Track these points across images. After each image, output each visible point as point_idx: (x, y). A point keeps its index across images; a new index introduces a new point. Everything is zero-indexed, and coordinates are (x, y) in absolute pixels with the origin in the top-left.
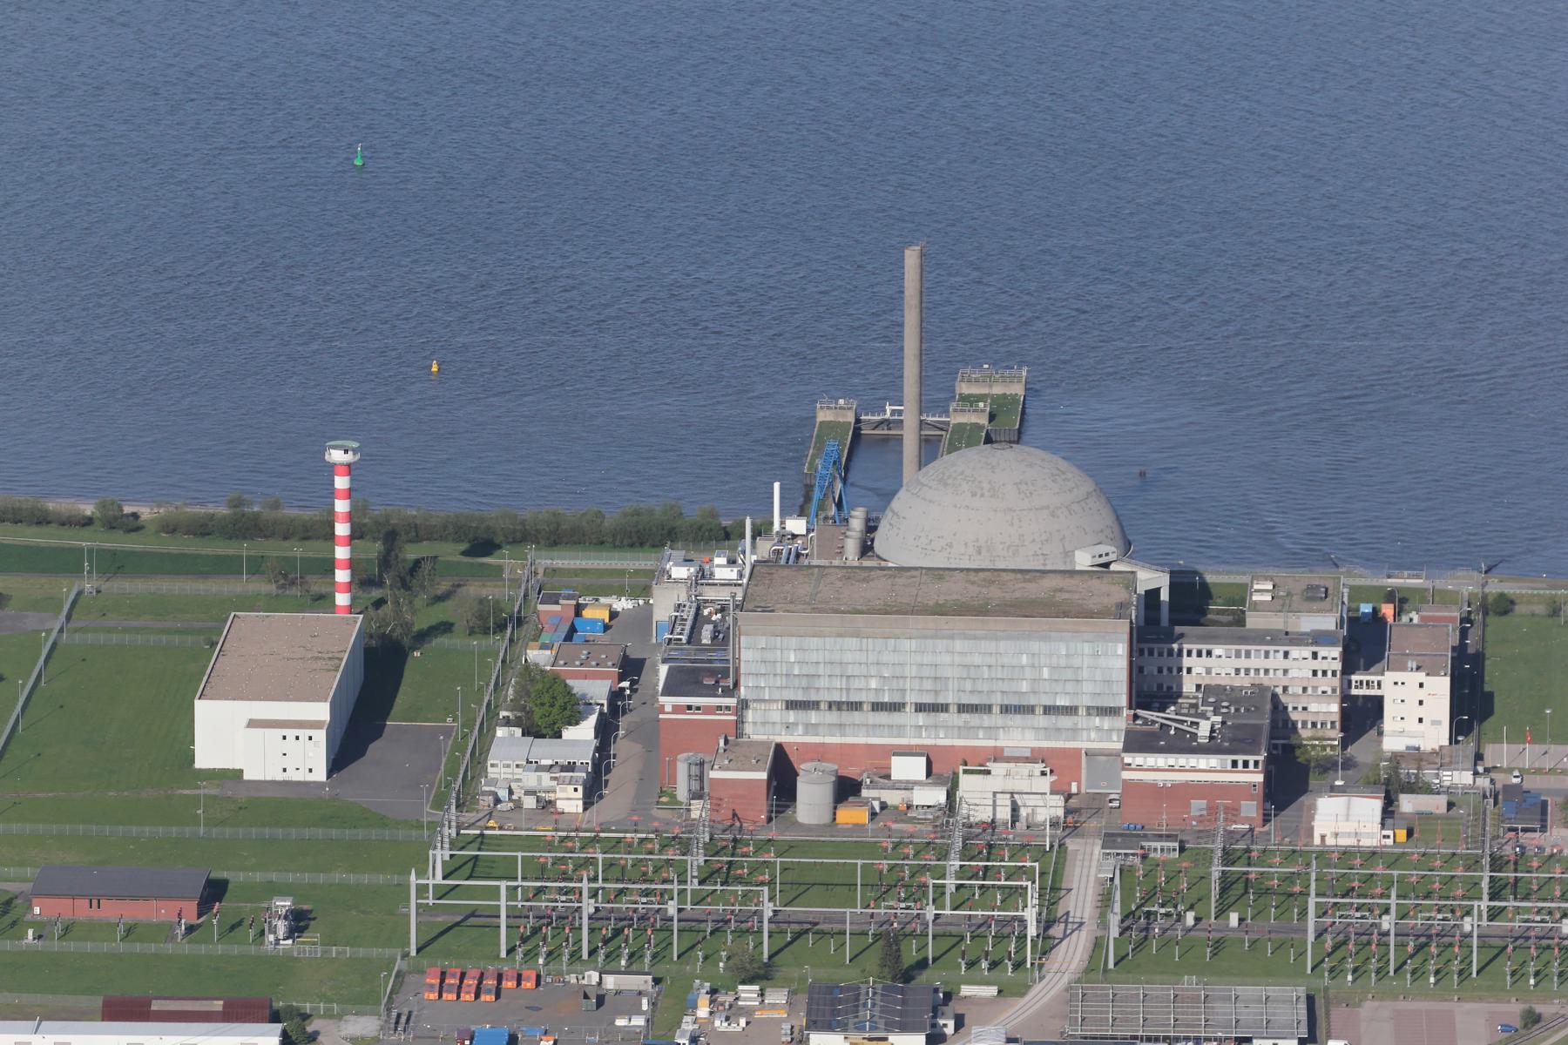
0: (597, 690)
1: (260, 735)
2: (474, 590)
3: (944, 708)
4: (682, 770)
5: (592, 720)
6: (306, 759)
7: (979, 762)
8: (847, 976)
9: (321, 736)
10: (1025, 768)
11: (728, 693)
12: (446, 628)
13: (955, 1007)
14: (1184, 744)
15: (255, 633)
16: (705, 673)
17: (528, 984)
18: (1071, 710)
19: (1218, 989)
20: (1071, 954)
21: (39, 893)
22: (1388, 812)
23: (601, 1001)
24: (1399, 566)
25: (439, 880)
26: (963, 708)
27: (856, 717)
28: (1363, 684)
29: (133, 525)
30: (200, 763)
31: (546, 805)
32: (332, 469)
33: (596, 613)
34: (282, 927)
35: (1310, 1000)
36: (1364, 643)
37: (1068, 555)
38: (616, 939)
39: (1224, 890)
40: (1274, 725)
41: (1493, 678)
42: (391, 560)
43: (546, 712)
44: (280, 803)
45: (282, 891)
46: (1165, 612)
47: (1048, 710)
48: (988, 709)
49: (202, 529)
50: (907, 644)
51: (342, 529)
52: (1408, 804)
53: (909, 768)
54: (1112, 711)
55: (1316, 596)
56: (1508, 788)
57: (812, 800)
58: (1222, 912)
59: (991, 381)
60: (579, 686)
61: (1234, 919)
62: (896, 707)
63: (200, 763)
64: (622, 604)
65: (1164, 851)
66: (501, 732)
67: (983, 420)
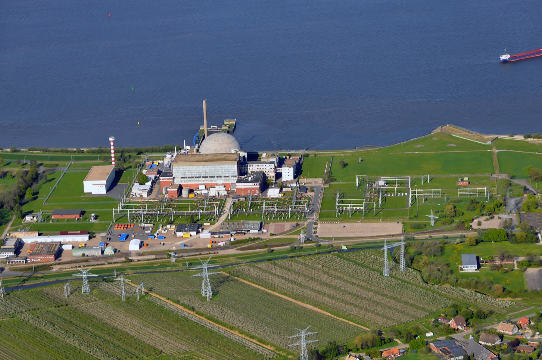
0: (153, 177)
1: (95, 186)
2: (137, 161)
3: (207, 177)
4: (164, 189)
5: (151, 181)
6: (102, 190)
7: (213, 186)
8: (184, 223)
9: (104, 186)
10: (221, 186)
11: (171, 176)
12: (131, 167)
13: (203, 227)
14: (246, 181)
15: (97, 169)
16: (169, 173)
17: (132, 226)
18: (228, 177)
19: (246, 222)
20: (223, 217)
21: (54, 214)
22: (281, 191)
23: (144, 228)
24: (290, 150)
25: (121, 209)
26: (210, 177)
27: (193, 179)
28: (279, 170)
29: (83, 152)
30: (85, 191)
31: (141, 196)
32: (110, 142)
33: (156, 163)
34: (92, 218)
35: (261, 223)
36: (281, 163)
37: (230, 150)
38: (147, 218)
39: (251, 205)
40: (264, 177)
41: (303, 168)
42: (122, 157)
43: (143, 180)
44: (99, 197)
45: (93, 212)
46: (246, 159)
47: (224, 177)
48: (214, 177)
49: (94, 152)
50: (200, 167)
51: (112, 151)
52: (284, 189)
53: (202, 187)
54: (235, 176)
55: (273, 155)
56: (302, 186)
57: (185, 193)
58: (250, 209)
59: (230, 121)
60: (149, 176)
61: (251, 210)
62: (200, 177)
63: (85, 191)
64: (161, 162)
65: (242, 199)
66: (135, 184)
67: (227, 128)
